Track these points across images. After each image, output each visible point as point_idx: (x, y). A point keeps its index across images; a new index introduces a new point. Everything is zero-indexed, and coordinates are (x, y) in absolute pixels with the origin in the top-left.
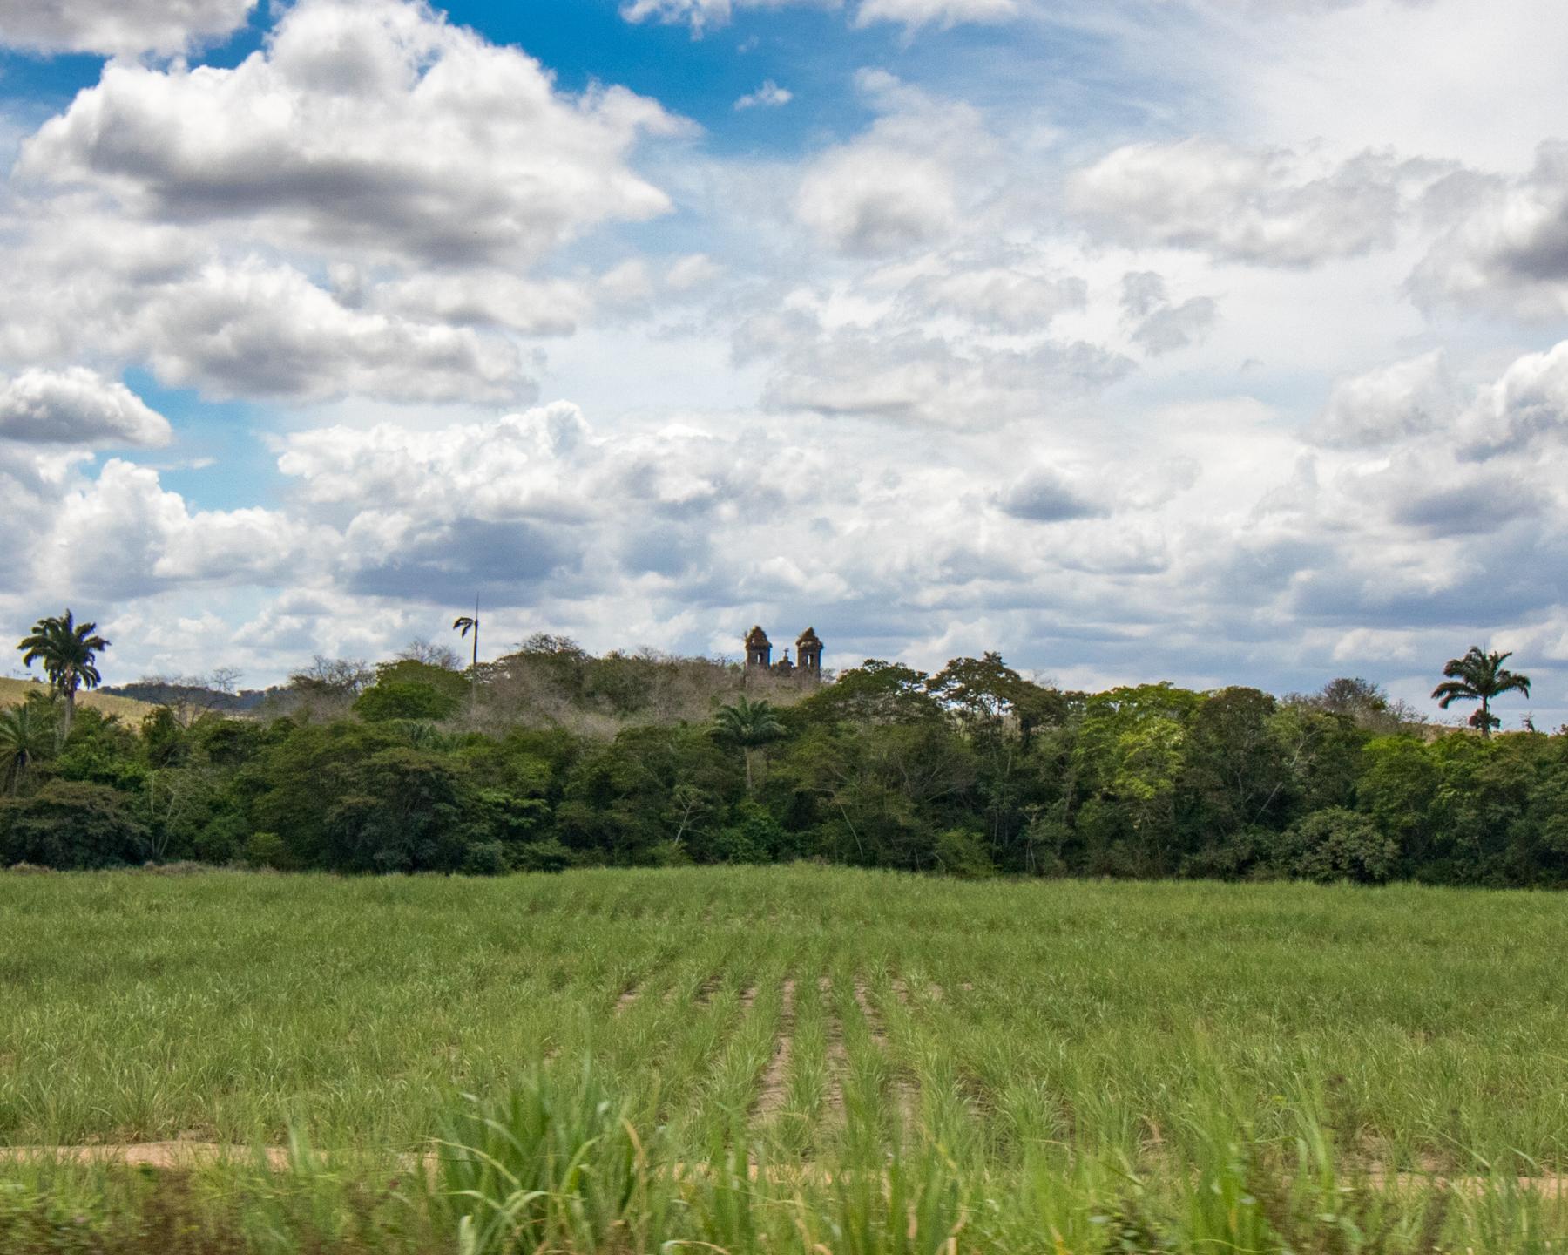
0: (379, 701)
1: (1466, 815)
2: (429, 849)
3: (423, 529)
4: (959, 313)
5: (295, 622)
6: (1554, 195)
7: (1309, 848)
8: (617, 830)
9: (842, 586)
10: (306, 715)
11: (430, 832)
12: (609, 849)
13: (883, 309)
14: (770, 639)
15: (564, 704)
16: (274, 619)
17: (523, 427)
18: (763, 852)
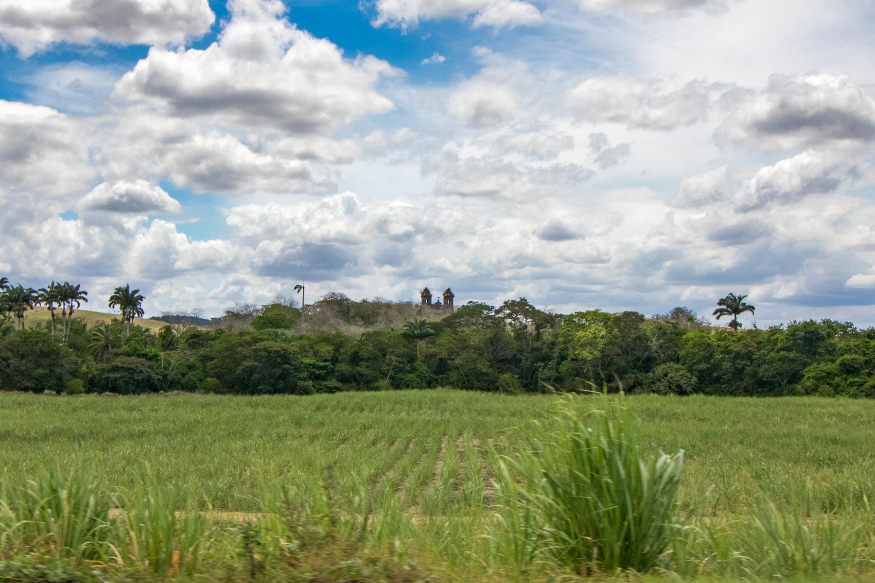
0: (262, 321)
1: (727, 365)
2: (281, 384)
3: (289, 248)
4: (519, 152)
5: (234, 288)
6: (777, 98)
7: (659, 380)
8: (362, 375)
9: (470, 270)
10: (230, 328)
11: (282, 377)
12: (358, 383)
13: (486, 151)
14: (432, 293)
15: (341, 322)
16: (226, 287)
17: (331, 203)
18: (424, 384)
